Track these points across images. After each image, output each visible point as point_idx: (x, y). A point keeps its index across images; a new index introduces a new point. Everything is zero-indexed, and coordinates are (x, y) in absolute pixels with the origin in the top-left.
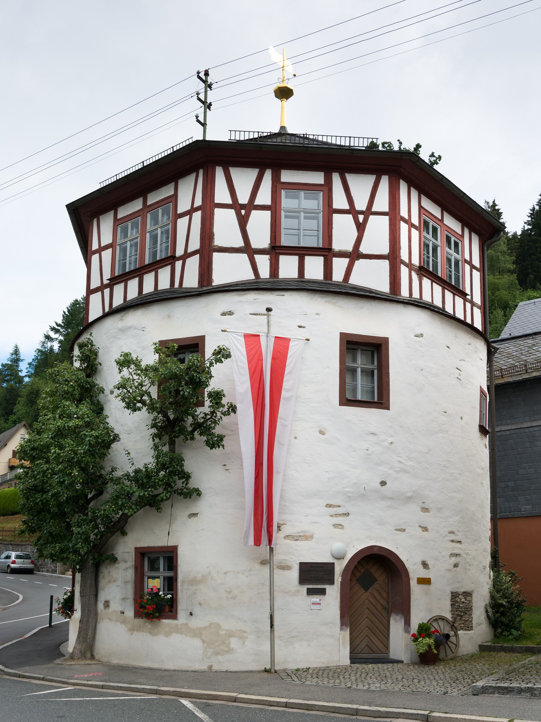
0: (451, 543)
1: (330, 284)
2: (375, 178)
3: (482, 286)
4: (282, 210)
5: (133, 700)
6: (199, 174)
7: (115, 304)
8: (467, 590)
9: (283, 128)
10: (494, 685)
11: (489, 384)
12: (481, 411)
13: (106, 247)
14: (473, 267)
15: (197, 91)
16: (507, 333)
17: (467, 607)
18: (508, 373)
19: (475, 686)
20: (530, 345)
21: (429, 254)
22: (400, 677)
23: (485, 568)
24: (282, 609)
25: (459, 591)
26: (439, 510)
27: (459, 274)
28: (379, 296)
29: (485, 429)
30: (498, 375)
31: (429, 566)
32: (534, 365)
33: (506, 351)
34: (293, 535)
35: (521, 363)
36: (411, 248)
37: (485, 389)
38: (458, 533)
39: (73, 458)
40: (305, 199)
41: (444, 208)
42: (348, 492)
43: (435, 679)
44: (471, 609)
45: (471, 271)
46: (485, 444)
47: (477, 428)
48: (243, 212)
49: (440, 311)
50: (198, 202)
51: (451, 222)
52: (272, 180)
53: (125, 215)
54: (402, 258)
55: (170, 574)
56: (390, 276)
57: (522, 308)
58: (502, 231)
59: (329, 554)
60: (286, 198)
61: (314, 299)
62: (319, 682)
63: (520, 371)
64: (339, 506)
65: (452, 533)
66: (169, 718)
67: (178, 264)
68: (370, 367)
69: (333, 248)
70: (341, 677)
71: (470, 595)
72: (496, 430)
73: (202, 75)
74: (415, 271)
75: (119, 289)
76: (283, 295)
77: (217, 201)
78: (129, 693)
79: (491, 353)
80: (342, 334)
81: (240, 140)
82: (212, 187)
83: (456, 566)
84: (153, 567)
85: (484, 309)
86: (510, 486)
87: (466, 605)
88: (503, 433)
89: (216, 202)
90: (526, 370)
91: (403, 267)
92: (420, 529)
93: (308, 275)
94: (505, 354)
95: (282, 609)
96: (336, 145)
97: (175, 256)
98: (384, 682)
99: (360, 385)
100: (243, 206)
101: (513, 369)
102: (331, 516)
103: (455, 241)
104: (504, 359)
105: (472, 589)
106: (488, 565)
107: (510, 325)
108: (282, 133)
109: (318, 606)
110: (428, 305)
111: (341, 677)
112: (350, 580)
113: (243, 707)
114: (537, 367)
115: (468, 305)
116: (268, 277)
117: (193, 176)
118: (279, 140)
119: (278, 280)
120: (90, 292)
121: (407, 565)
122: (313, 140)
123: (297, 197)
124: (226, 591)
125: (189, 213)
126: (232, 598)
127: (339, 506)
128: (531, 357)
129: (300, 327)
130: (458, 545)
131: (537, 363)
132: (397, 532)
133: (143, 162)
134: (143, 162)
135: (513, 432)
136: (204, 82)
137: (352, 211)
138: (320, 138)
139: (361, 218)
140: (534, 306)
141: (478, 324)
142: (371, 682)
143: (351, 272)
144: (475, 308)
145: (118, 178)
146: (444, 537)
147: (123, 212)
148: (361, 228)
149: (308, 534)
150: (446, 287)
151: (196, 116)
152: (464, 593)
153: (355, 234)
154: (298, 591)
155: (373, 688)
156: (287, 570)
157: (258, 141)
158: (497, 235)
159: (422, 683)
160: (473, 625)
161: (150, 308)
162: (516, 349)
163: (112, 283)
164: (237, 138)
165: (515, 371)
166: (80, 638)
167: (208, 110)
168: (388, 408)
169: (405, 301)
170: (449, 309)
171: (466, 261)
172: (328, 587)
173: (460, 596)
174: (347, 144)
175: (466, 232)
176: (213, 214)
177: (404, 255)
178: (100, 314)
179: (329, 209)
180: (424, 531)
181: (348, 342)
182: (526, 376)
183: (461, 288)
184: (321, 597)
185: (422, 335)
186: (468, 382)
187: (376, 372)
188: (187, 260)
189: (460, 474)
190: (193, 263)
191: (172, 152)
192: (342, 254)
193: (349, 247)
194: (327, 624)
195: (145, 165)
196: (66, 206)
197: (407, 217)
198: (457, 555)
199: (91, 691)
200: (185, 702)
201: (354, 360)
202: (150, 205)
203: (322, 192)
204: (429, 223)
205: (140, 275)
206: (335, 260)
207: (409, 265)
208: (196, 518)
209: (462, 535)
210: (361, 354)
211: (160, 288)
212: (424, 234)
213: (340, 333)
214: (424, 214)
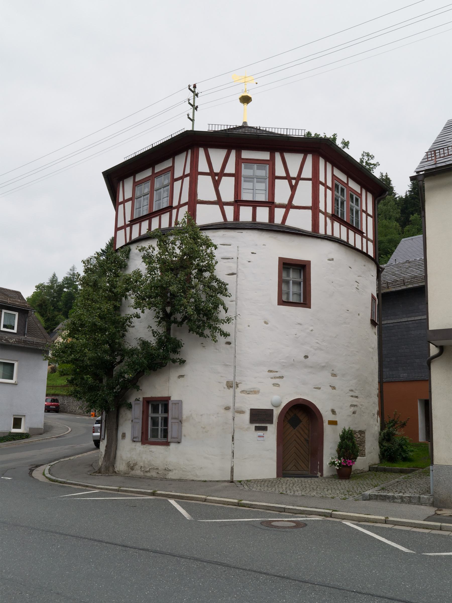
0: (351, 398)
1: (272, 225)
2: (303, 156)
3: (374, 227)
4: (242, 177)
5: (137, 499)
6: (189, 152)
7: (133, 237)
8: (361, 429)
9: (245, 123)
10: (377, 494)
11: (378, 293)
12: (372, 310)
13: (128, 200)
14: (368, 215)
15: (188, 98)
16: (393, 259)
17: (361, 441)
18: (392, 285)
19: (364, 494)
20: (407, 267)
22: (315, 487)
23: (374, 415)
24: (238, 440)
25: (356, 430)
26: (343, 375)
27: (358, 219)
28: (305, 233)
29: (375, 322)
30: (385, 286)
31: (336, 412)
32: (409, 280)
33: (391, 271)
35: (401, 278)
36: (326, 202)
37: (375, 296)
38: (356, 391)
40: (257, 169)
41: (349, 176)
42: (283, 362)
43: (338, 489)
44: (364, 442)
45: (367, 218)
46: (375, 332)
47: (369, 322)
48: (217, 178)
49: (345, 244)
50: (188, 171)
51: (353, 185)
52: (236, 157)
53: (141, 179)
54: (321, 209)
55: (165, 415)
57: (404, 242)
58: (387, 191)
59: (270, 404)
60: (244, 169)
61: (262, 235)
62: (261, 489)
63: (400, 284)
64: (277, 372)
65: (352, 391)
66: (159, 512)
67: (174, 211)
69: (275, 202)
70: (276, 486)
71: (364, 433)
72: (383, 323)
74: (329, 217)
75: (136, 227)
77: (200, 170)
78: (136, 495)
79: (379, 271)
80: (280, 258)
81: (215, 131)
83: (354, 413)
84: (155, 410)
85: (375, 242)
86: (393, 360)
87: (361, 440)
88: (388, 325)
89: (199, 171)
91: (320, 214)
92: (331, 388)
93: (259, 220)
94: (390, 272)
95: (238, 440)
96: (278, 134)
97: (172, 206)
98: (304, 490)
99: (291, 291)
100: (217, 174)
101: (396, 283)
102: (272, 378)
103: (356, 198)
104: (390, 276)
105: (365, 429)
106: (376, 413)
107: (396, 253)
108: (244, 126)
109: (262, 438)
110: (338, 240)
111: (276, 486)
112: (284, 421)
113: (209, 505)
114: (411, 282)
115: (364, 240)
116: (233, 221)
117: (185, 153)
118: (240, 131)
119: (239, 222)
120: (117, 229)
121: (322, 412)
122: (263, 130)
123: (251, 168)
124: (202, 427)
125: (182, 178)
126: (205, 432)
127: (277, 372)
128: (408, 275)
129: (252, 253)
130: (356, 399)
131: (411, 279)
132: (315, 389)
133: (152, 144)
134: (152, 144)
135: (395, 324)
136: (193, 92)
137: (288, 177)
138: (267, 130)
139: (294, 182)
140: (412, 241)
141: (371, 253)
142: (296, 490)
143: (287, 217)
144: (369, 242)
145: (136, 155)
146: (346, 394)
147: (140, 177)
148: (293, 188)
149: (256, 390)
150: (349, 228)
151: (187, 115)
152: (360, 431)
153: (289, 192)
154: (249, 428)
155: (297, 493)
156: (242, 413)
157: (227, 131)
159: (330, 491)
160: (366, 453)
162: (398, 269)
163: (132, 224)
164: (214, 129)
165: (397, 284)
166: (105, 458)
167: (195, 110)
168: (310, 308)
169: (322, 237)
170: (351, 242)
171: (363, 211)
172: (268, 425)
173: (357, 433)
174: (285, 134)
175: (364, 191)
176: (197, 179)
177: (322, 207)
178: (124, 243)
179: (272, 176)
180: (333, 389)
181: (285, 264)
183: (360, 229)
184: (264, 432)
185: (333, 259)
186: (363, 291)
187: (302, 283)
188: (180, 209)
189: (357, 352)
190: (184, 210)
191: (171, 138)
193: (285, 201)
194: (268, 450)
195: (154, 146)
196: (102, 173)
197: (324, 182)
198: (355, 405)
199: (110, 493)
200: (172, 502)
201: (288, 275)
202: (157, 173)
203: (268, 165)
204: (339, 185)
205: (149, 218)
206: (277, 210)
207: (325, 214)
208: (183, 378)
209: (359, 392)
210: (292, 271)
211: (162, 227)
212: (336, 193)
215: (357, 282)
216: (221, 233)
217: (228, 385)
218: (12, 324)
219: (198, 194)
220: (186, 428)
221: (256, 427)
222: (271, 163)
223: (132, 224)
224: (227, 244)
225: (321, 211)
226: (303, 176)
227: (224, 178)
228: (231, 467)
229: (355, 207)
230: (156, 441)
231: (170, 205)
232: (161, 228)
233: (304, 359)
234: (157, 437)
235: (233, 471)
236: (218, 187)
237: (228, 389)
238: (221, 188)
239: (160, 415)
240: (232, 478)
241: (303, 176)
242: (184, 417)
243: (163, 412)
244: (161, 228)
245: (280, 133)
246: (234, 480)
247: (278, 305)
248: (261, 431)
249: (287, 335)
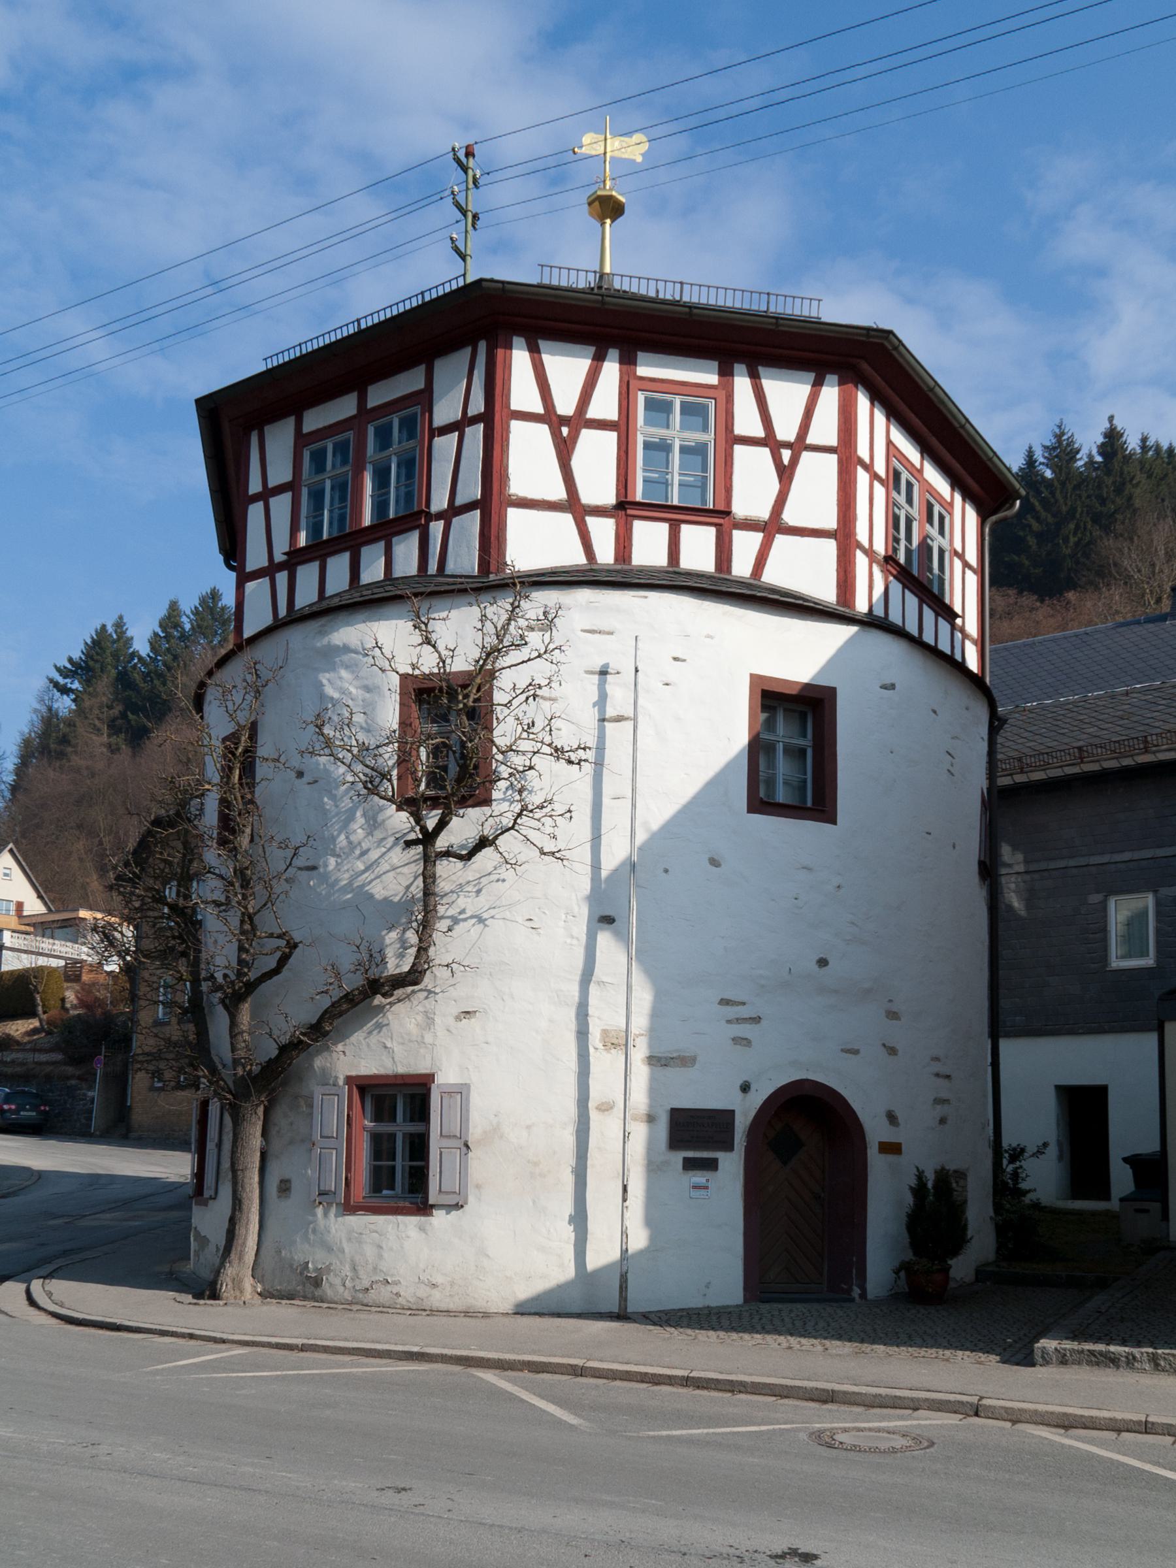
4: (638, 433)
6: (479, 349)
13: (280, 489)
21: (898, 533)
34: (660, 1055)
41: (926, 450)
45: (964, 573)
48: (565, 431)
56: (837, 570)
64: (744, 1004)
67: (437, 528)
68: (801, 742)
73: (461, 155)
74: (878, 563)
75: (307, 575)
76: (646, 597)
80: (755, 679)
82: (506, 378)
83: (943, 1121)
90: (1022, 768)
91: (859, 553)
100: (565, 420)
102: (729, 1022)
109: (703, 1192)
125: (457, 427)
127: (744, 1004)
129: (675, 659)
137: (769, 441)
139: (786, 455)
143: (766, 560)
145: (304, 352)
147: (315, 420)
148: (785, 474)
150: (924, 598)
153: (774, 486)
158: (1008, 505)
161: (381, 610)
163: (294, 561)
171: (956, 553)
172: (720, 1155)
177: (862, 535)
178: (268, 620)
182: (1020, 778)
185: (892, 687)
191: (420, 302)
192: (749, 525)
193: (763, 512)
195: (363, 326)
205: (352, 546)
207: (870, 553)
213: (752, 675)
214: (895, 457)
215: (950, 754)
216: (584, 595)
217: (607, 1040)
219: (511, 477)
220: (480, 1165)
221: (686, 1160)
222: (721, 394)
223: (294, 561)
224: (602, 629)
225: (859, 546)
226: (811, 439)
227: (586, 434)
228: (622, 1276)
229: (937, 542)
232: (361, 584)
233: (816, 967)
235: (626, 1287)
236: (570, 460)
238: (577, 462)
239: (401, 1128)
240: (623, 1306)
241: (811, 439)
243: (408, 1119)
244: (361, 584)
246: (629, 1310)
247: (749, 812)
248: (699, 1173)
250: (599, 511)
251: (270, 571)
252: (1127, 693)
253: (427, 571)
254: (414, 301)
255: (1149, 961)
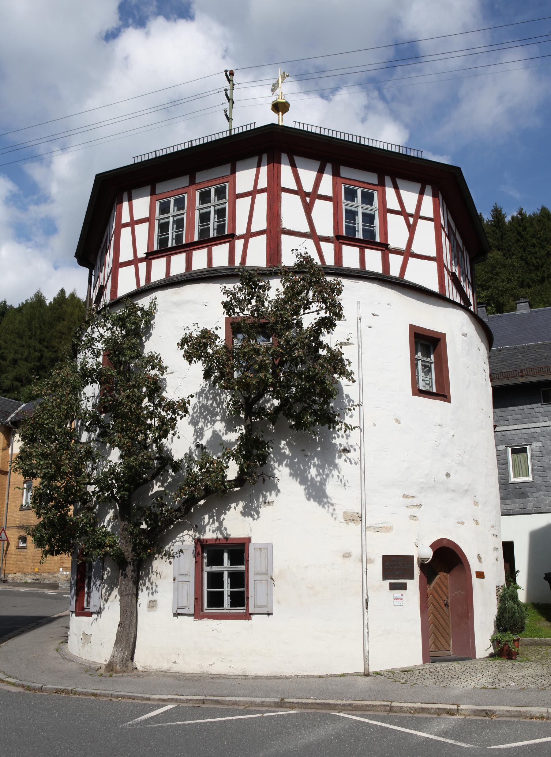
6: (263, 159)
39: (27, 454)
48: (308, 199)
67: (239, 244)
84: (216, 560)
100: (307, 194)
102: (407, 507)
109: (400, 602)
125: (253, 194)
129: (374, 314)
133: (191, 141)
134: (191, 141)
137: (402, 212)
139: (411, 220)
145: (158, 155)
148: (412, 229)
151: (224, 110)
191: (228, 135)
195: (194, 145)
203: (377, 192)
217: (347, 517)
218: (505, 308)
221: (391, 584)
226: (421, 214)
230: (223, 613)
231: (231, 233)
234: (221, 604)
236: (311, 213)
237: (346, 525)
242: (276, 572)
245: (390, 150)
249: (426, 442)
250: (326, 239)
251: (135, 262)
252: (500, 350)
253: (234, 263)
254: (224, 134)
255: (530, 479)
